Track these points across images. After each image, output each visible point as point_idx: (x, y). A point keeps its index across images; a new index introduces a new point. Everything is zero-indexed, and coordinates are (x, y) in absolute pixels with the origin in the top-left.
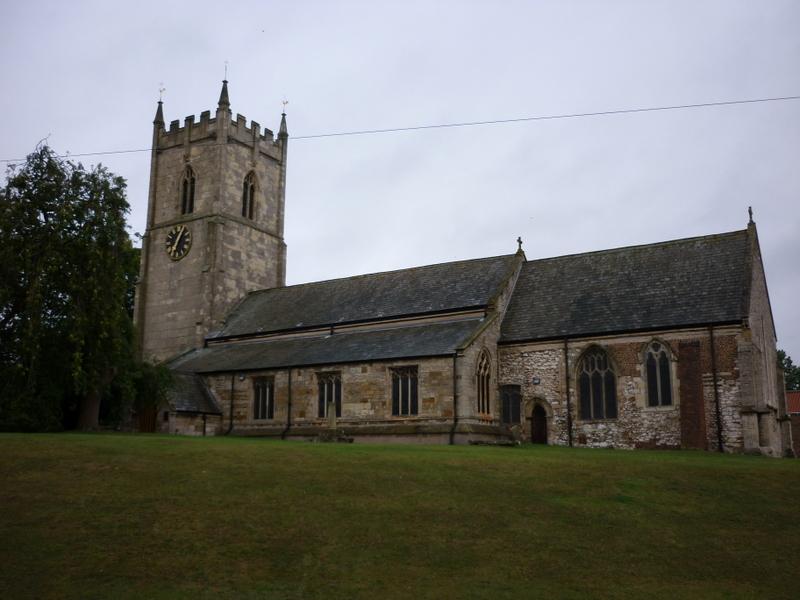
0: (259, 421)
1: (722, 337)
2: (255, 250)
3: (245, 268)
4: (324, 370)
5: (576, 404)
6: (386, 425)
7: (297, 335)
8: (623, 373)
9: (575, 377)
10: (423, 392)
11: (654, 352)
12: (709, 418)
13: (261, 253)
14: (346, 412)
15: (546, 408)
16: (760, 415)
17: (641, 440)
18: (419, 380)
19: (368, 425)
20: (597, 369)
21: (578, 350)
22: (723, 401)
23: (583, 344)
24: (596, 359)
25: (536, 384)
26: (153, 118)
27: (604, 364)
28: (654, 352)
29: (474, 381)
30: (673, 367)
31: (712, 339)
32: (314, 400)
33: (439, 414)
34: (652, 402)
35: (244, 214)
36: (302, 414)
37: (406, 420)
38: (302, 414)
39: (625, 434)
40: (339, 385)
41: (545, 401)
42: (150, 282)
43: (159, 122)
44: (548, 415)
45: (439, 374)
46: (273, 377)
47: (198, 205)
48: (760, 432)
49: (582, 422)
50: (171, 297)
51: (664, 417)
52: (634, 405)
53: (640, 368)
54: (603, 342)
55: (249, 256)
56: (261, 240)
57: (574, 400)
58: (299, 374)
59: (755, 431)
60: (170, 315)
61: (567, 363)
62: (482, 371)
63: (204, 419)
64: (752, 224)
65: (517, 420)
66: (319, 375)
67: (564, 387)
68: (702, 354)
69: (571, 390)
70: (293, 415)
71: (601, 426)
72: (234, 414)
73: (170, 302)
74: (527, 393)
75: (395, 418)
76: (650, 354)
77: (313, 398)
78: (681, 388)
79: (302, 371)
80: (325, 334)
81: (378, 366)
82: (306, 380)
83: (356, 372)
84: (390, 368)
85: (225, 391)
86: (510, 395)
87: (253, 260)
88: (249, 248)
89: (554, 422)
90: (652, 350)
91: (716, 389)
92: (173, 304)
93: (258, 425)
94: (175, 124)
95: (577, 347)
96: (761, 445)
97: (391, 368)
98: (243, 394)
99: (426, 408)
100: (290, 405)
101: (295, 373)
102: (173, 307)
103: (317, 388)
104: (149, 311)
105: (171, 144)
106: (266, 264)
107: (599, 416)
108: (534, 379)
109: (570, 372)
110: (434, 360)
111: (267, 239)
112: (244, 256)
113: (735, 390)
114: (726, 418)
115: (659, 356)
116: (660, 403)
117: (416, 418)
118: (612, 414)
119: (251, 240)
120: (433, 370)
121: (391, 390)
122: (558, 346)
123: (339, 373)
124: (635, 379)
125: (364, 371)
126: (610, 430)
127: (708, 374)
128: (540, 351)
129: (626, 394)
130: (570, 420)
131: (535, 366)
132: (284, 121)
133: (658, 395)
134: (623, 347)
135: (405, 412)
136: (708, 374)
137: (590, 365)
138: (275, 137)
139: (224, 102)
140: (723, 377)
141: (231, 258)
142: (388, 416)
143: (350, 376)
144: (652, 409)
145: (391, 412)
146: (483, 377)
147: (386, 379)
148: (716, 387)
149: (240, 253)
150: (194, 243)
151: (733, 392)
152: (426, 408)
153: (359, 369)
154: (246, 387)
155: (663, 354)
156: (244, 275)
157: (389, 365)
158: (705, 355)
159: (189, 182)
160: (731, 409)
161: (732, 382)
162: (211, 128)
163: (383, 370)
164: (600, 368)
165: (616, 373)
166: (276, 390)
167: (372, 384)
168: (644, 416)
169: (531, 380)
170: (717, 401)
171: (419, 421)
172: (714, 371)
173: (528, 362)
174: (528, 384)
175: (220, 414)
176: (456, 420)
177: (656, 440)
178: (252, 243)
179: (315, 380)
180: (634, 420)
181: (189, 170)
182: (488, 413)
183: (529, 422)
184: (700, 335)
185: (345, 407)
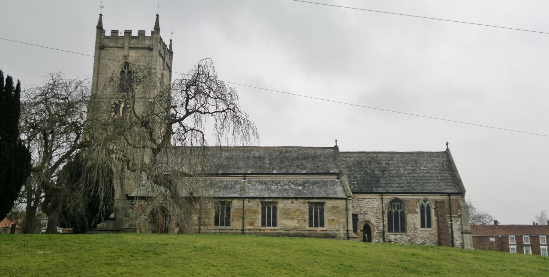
0: (219, 227)
1: (453, 199)
4: (266, 200)
6: (307, 232)
8: (410, 212)
10: (327, 216)
15: (371, 226)
19: (295, 232)
21: (388, 199)
22: (454, 227)
25: (365, 214)
26: (96, 24)
27: (399, 207)
30: (433, 211)
31: (450, 200)
32: (259, 217)
34: (423, 226)
36: (251, 224)
37: (268, 229)
38: (251, 224)
39: (410, 240)
40: (275, 209)
41: (371, 223)
43: (100, 28)
44: (372, 229)
45: (337, 207)
51: (428, 233)
52: (415, 227)
53: (418, 210)
54: (400, 197)
57: (386, 223)
58: (249, 202)
64: (448, 149)
67: (381, 216)
69: (384, 218)
70: (245, 224)
72: (202, 223)
75: (311, 228)
77: (259, 215)
79: (251, 200)
81: (302, 201)
83: (287, 203)
89: (375, 233)
90: (423, 203)
93: (220, 230)
94: (114, 32)
95: (388, 198)
97: (309, 203)
99: (45, 223)
100: (243, 219)
101: (246, 201)
107: (397, 230)
108: (365, 212)
109: (384, 210)
110: (334, 200)
116: (272, 226)
117: (324, 229)
118: (404, 230)
120: (333, 205)
122: (378, 197)
123: (276, 203)
124: (416, 215)
125: (293, 203)
128: (368, 198)
129: (411, 221)
130: (384, 232)
131: (365, 205)
132: (157, 19)
133: (426, 222)
134: (409, 200)
137: (393, 207)
139: (157, 28)
140: (454, 217)
142: (308, 228)
144: (423, 229)
147: (305, 208)
148: (451, 221)
151: (458, 224)
152: (45, 223)
153: (289, 201)
155: (428, 205)
157: (308, 201)
160: (457, 231)
161: (458, 219)
162: (147, 43)
163: (304, 203)
165: (406, 212)
166: (232, 210)
169: (363, 212)
170: (452, 227)
172: (450, 214)
173: (362, 203)
179: (260, 206)
180: (415, 234)
183: (362, 232)
184: (445, 198)
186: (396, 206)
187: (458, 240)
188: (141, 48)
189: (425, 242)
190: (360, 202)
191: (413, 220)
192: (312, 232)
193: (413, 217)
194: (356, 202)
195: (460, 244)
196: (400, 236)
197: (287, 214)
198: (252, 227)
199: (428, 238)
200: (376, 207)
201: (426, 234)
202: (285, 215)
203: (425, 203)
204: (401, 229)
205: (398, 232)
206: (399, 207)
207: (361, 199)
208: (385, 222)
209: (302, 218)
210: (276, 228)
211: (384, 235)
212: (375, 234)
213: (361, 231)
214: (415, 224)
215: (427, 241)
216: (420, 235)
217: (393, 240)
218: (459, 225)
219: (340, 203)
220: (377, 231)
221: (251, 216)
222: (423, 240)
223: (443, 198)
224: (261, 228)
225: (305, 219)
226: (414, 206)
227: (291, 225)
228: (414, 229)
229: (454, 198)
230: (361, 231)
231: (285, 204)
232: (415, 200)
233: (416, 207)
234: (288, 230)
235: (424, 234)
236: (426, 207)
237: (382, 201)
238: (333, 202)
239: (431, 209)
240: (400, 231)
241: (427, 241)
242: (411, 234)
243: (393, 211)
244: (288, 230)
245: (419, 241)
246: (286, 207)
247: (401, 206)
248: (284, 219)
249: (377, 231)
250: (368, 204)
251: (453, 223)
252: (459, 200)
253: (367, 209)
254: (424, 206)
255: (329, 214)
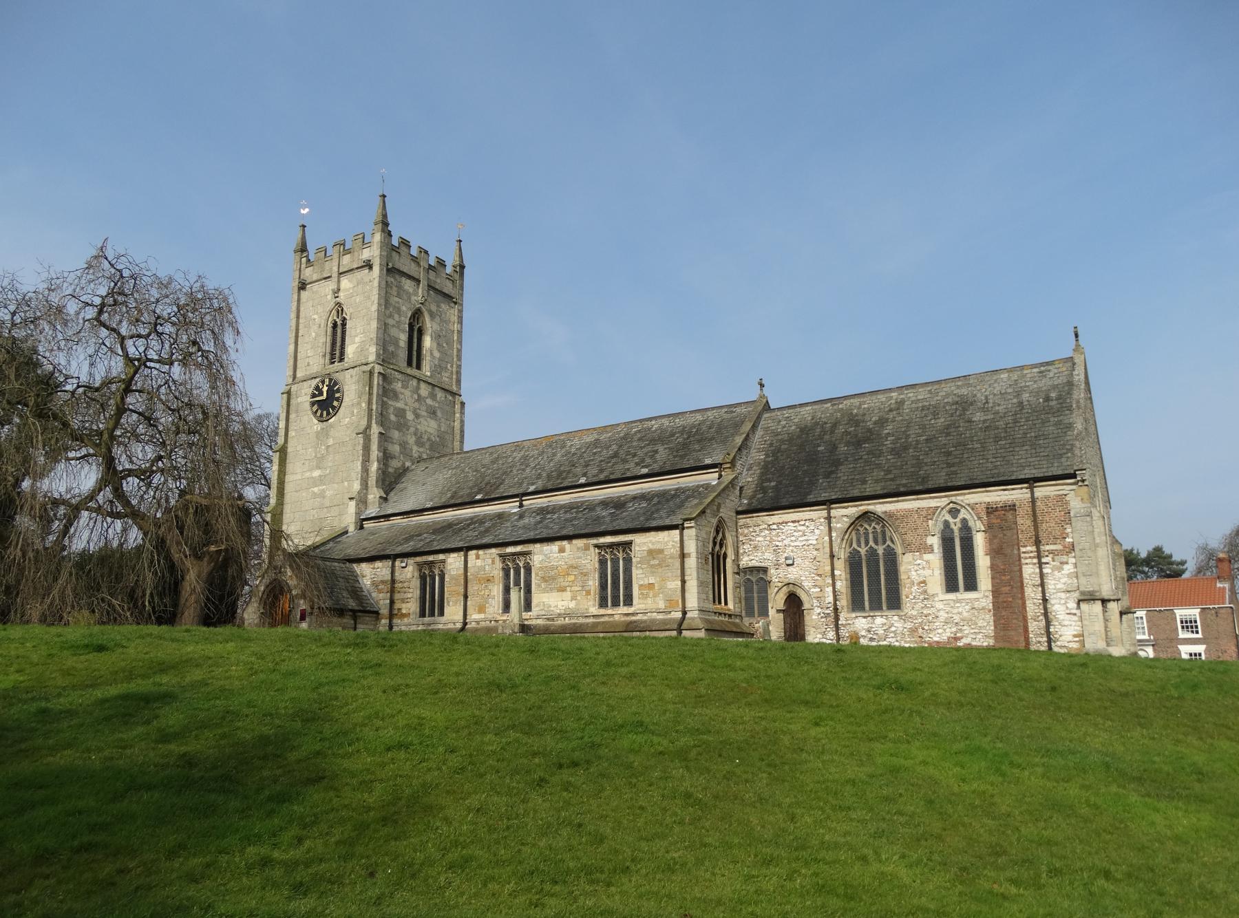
0: (427, 619)
1: (1047, 497)
2: (424, 408)
3: (412, 430)
4: (510, 550)
5: (844, 590)
7: (477, 509)
8: (908, 548)
9: (842, 554)
10: (639, 576)
11: (951, 520)
12: (1033, 607)
13: (432, 413)
14: (537, 605)
15: (803, 597)
16: (1104, 602)
17: (936, 639)
18: (634, 560)
20: (871, 543)
21: (845, 519)
22: (1051, 585)
23: (853, 510)
24: (870, 530)
28: (951, 520)
29: (706, 559)
30: (980, 541)
31: (1033, 500)
32: (497, 590)
33: (661, 605)
34: (951, 586)
35: (410, 364)
36: (481, 609)
38: (481, 609)
40: (528, 569)
42: (289, 450)
44: (806, 606)
45: (661, 551)
46: (443, 561)
47: (350, 350)
48: (1106, 627)
49: (854, 615)
50: (318, 467)
53: (935, 541)
55: (417, 416)
56: (433, 396)
57: (842, 585)
59: (1099, 626)
60: (316, 490)
61: (831, 537)
62: (717, 548)
63: (355, 618)
65: (764, 612)
66: (503, 557)
67: (828, 568)
68: (1020, 521)
69: (836, 572)
71: (879, 621)
73: (316, 473)
74: (776, 576)
76: (946, 524)
78: (993, 567)
79: (481, 552)
80: (511, 507)
81: (579, 543)
82: (486, 563)
84: (596, 546)
85: (383, 582)
86: (754, 580)
87: (422, 420)
88: (416, 405)
90: (948, 517)
91: (1041, 568)
92: (320, 476)
96: (1108, 645)
97: (500, 556)
98: (406, 585)
100: (466, 597)
101: (472, 554)
102: (321, 480)
103: (501, 574)
104: (289, 488)
105: (315, 277)
106: (439, 426)
107: (876, 606)
108: (786, 558)
109: (836, 549)
111: (440, 395)
112: (410, 416)
113: (1068, 568)
114: (1056, 607)
115: (959, 525)
116: (622, 604)
117: (631, 610)
118: (895, 603)
119: (419, 396)
120: (651, 546)
121: (597, 576)
122: (818, 514)
124: (927, 557)
125: (562, 550)
126: (892, 625)
127: (1029, 548)
128: (793, 522)
135: (616, 604)
136: (1029, 548)
138: (449, 270)
140: (1051, 552)
141: (393, 418)
142: (594, 610)
143: (544, 556)
144: (952, 596)
145: (597, 604)
146: (718, 557)
148: (1041, 565)
149: (404, 411)
150: (346, 399)
152: (644, 596)
153: (555, 547)
154: (409, 575)
156: (411, 440)
157: (594, 541)
158: (1024, 522)
159: (339, 322)
160: (1063, 595)
161: (1064, 558)
164: (876, 542)
166: (447, 579)
167: (572, 566)
168: (940, 605)
171: (633, 614)
172: (1038, 543)
173: (777, 535)
174: (777, 566)
175: (377, 613)
176: (684, 613)
177: (956, 639)
178: (420, 399)
179: (499, 564)
181: (339, 309)
182: (726, 603)
184: (1018, 494)
185: (536, 598)
186: (871, 536)
187: (1066, 623)
188: (357, 268)
189: (958, 635)
190: (774, 533)
191: (921, 572)
192: (602, 620)
193: (919, 562)
194: (763, 534)
195: (1075, 636)
196: (885, 621)
197: (553, 581)
198: (482, 616)
199: (968, 621)
200: (815, 542)
201: (960, 610)
202: (546, 581)
203: (955, 517)
204: (888, 599)
205: (880, 608)
206: (880, 536)
207: (775, 527)
208: (839, 584)
209: (583, 586)
210: (631, 610)
211: (837, 618)
212: (814, 617)
213: (779, 611)
214: (924, 582)
215: (967, 630)
216: (943, 616)
217: (863, 633)
218: (1069, 576)
219: (666, 539)
220: (819, 610)
221: (481, 591)
222: (954, 630)
223: (1013, 497)
224: (499, 618)
225: (587, 588)
226: (920, 531)
227: (560, 607)
228: (922, 597)
229: (1048, 494)
230: (779, 611)
231: (546, 555)
232: (924, 513)
233: (927, 533)
234: (553, 620)
235: (955, 611)
236: (956, 529)
237: (830, 523)
238: (651, 538)
239: (974, 532)
240: (884, 608)
241: (967, 630)
242: (914, 613)
243: (863, 551)
244: (553, 620)
245: (940, 631)
246: (550, 563)
247: (884, 533)
248: (545, 591)
249: (819, 610)
250: (793, 538)
251: (1045, 571)
252: (1067, 498)
253: (792, 551)
254: (953, 526)
255: (641, 571)
